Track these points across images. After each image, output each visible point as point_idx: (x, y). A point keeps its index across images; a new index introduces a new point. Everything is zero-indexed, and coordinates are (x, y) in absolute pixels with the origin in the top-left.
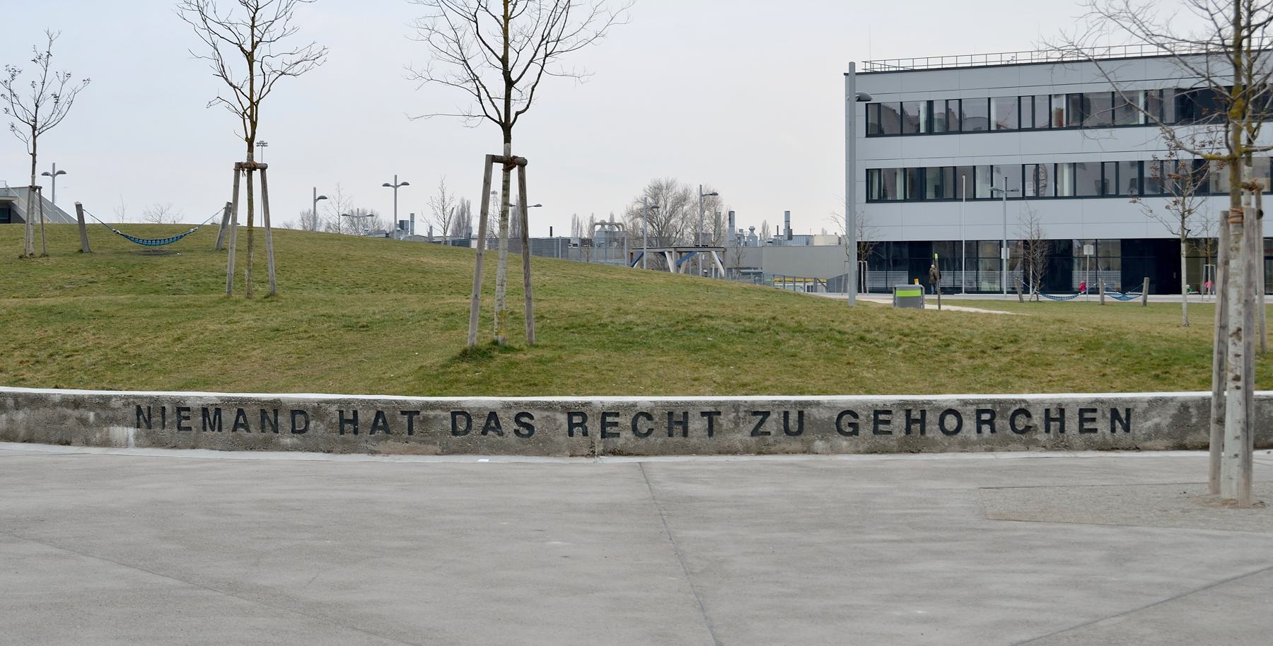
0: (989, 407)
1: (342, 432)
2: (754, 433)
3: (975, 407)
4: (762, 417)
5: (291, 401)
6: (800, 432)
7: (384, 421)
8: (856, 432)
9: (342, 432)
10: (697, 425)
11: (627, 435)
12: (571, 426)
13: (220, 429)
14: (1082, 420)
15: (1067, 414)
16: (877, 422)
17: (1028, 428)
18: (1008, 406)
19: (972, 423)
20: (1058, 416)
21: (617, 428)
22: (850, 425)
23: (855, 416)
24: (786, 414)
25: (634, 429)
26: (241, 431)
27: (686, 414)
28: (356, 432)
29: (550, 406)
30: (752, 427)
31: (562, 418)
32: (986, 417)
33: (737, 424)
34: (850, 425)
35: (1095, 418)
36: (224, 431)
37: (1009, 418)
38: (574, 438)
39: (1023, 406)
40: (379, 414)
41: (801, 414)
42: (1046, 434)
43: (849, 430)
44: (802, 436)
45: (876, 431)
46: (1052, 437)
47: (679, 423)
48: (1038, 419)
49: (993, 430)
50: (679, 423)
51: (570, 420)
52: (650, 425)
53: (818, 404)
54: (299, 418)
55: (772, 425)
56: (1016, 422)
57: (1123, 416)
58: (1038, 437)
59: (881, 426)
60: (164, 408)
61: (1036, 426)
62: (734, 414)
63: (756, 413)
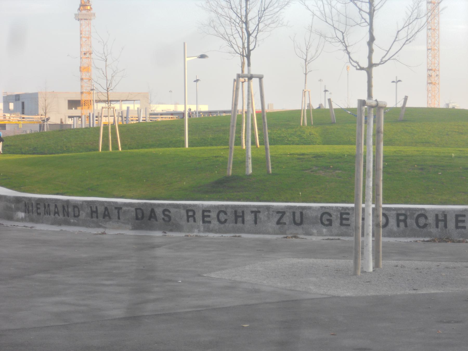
0: (403, 212)
1: (92, 217)
2: (278, 223)
3: (395, 212)
4: (281, 214)
5: (73, 200)
6: (301, 223)
7: (108, 213)
8: (330, 224)
9: (92, 217)
10: (249, 218)
11: (215, 223)
12: (188, 217)
13: (50, 215)
14: (457, 221)
15: (448, 218)
16: (342, 219)
17: (425, 226)
18: (414, 212)
19: (394, 221)
20: (443, 218)
21: (209, 218)
22: (328, 220)
23: (330, 215)
24: (294, 213)
25: (219, 220)
26: (57, 215)
27: (243, 212)
28: (97, 217)
29: (177, 206)
30: (276, 219)
31: (183, 212)
32: (402, 218)
33: (269, 218)
34: (328, 220)
35: (465, 220)
36: (51, 215)
37: (415, 219)
38: (189, 223)
39: (423, 212)
40: (106, 209)
41: (301, 213)
42: (436, 229)
43: (326, 223)
44: (302, 226)
45: (341, 224)
46: (440, 230)
47: (442, 220)
48: (431, 220)
49: (406, 226)
50: (442, 220)
51: (187, 213)
52: (225, 217)
53: (310, 208)
54: (76, 209)
55: (287, 219)
56: (419, 221)
57: (46, 213)
58: (432, 230)
59: (344, 221)
60: (32, 203)
61: (430, 224)
62: (267, 213)
63: (278, 212)
